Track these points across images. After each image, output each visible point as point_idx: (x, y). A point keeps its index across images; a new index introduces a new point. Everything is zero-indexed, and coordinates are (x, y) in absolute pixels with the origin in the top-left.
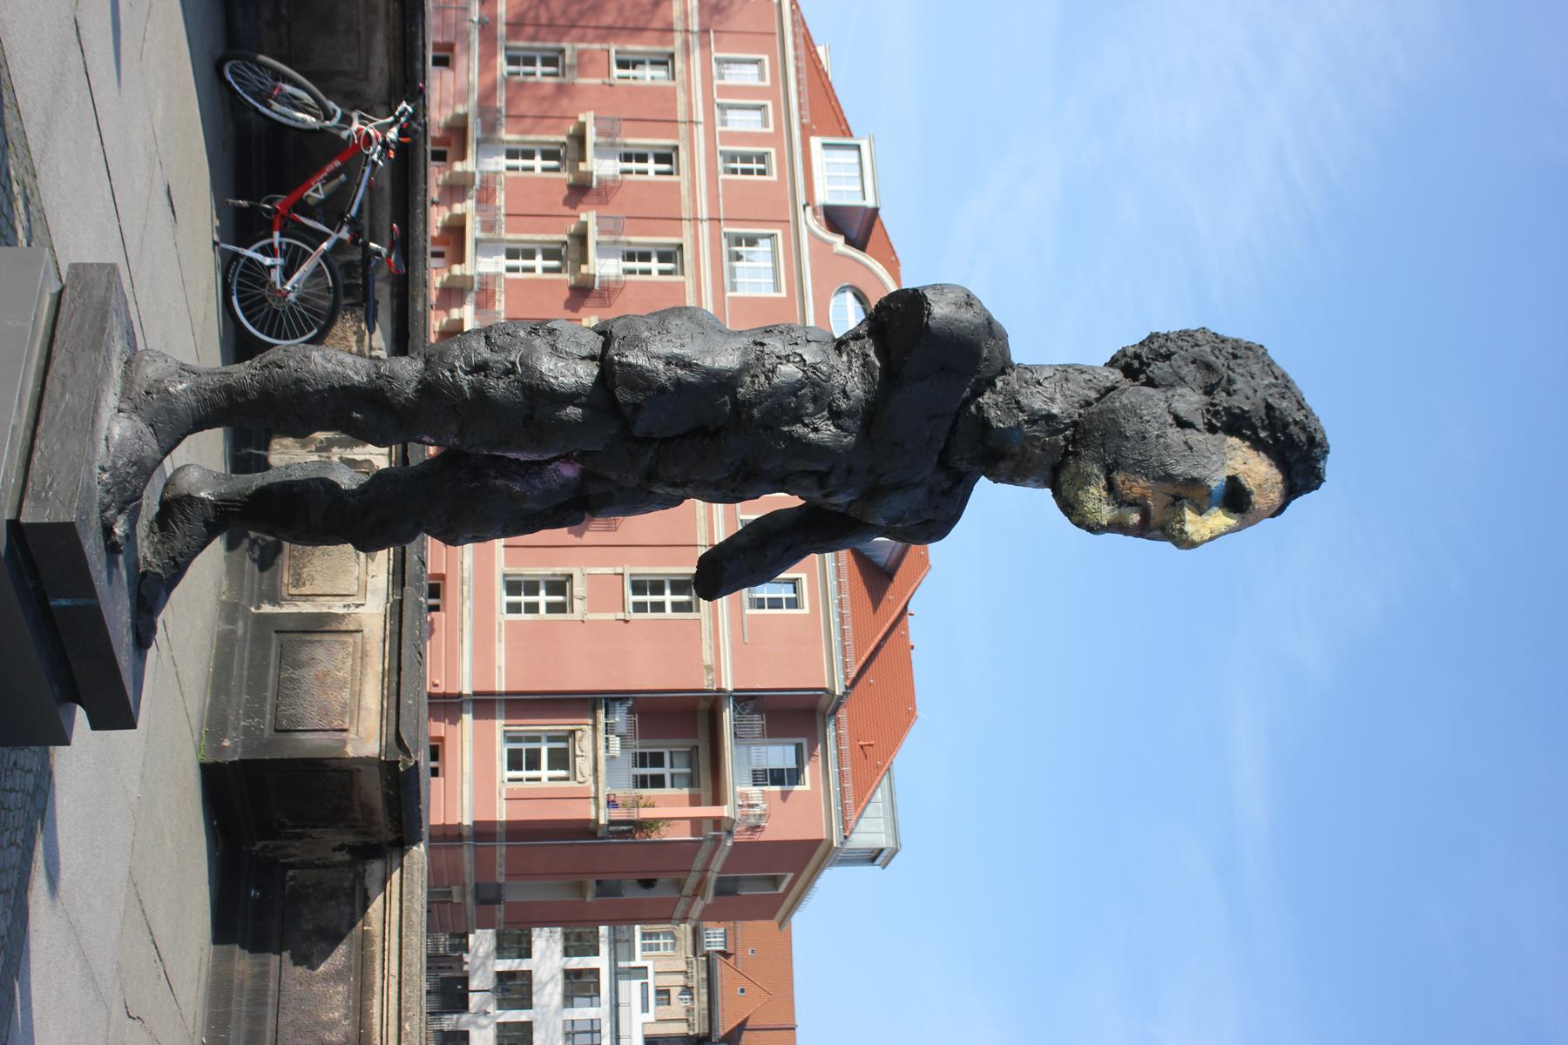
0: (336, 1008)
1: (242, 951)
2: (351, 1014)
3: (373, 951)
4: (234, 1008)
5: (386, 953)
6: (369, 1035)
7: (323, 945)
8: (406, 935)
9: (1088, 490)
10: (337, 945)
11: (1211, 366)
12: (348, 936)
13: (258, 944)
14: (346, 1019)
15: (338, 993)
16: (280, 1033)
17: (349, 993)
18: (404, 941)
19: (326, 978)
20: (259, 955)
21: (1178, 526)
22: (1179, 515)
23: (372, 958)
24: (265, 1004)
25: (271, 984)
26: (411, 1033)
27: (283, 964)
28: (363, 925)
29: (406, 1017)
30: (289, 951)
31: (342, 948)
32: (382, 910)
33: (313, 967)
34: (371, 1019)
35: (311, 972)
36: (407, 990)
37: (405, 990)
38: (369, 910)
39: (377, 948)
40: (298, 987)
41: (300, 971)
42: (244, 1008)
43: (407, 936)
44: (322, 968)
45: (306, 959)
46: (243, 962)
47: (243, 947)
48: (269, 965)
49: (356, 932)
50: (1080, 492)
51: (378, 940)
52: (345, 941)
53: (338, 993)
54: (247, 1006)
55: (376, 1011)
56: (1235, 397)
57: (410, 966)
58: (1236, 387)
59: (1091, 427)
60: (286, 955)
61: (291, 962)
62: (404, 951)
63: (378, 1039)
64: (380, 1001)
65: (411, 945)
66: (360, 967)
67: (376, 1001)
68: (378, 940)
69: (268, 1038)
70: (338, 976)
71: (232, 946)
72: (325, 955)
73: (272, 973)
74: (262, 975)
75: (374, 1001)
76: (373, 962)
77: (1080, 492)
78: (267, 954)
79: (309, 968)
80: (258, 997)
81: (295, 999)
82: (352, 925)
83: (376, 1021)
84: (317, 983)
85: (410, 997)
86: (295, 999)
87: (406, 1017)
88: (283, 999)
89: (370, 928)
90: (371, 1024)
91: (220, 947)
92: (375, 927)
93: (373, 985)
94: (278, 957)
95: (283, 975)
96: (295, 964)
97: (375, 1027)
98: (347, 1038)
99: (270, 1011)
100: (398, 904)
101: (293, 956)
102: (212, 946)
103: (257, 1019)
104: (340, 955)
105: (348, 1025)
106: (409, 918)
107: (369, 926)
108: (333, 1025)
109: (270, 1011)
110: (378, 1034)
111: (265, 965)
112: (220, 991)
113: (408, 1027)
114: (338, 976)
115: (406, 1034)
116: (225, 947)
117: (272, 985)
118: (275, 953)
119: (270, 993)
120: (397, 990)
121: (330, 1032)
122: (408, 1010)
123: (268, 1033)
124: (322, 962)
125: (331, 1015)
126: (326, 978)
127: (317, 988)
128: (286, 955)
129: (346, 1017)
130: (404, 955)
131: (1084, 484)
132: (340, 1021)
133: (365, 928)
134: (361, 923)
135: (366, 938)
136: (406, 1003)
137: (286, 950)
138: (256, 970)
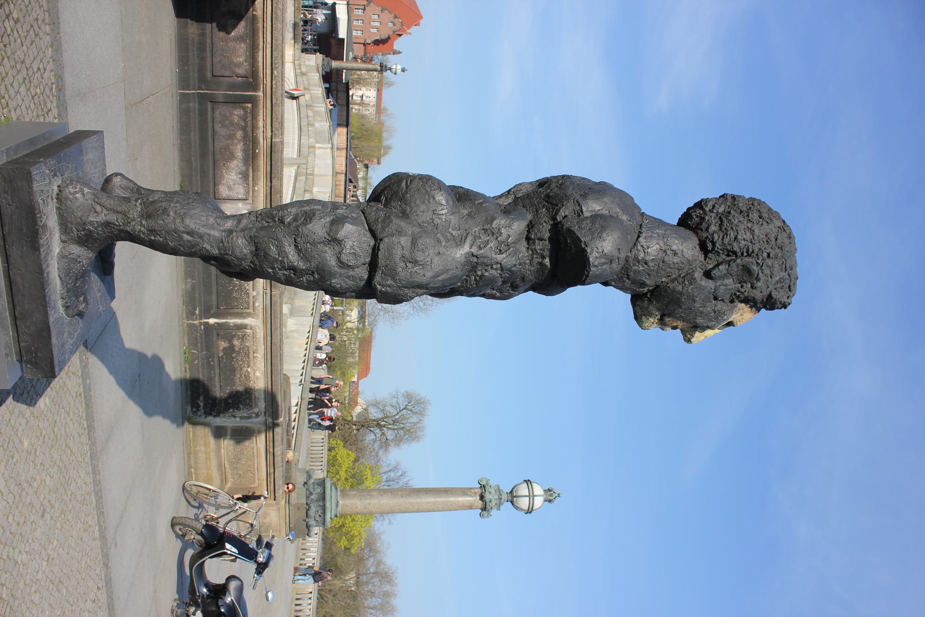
0: (241, 56)
1: (192, 22)
2: (248, 60)
3: (258, 26)
4: (190, 54)
5: (265, 29)
6: (257, 71)
7: (233, 20)
8: (275, 23)
9: (649, 319)
10: (240, 22)
11: (751, 272)
12: (246, 17)
13: (200, 18)
14: (246, 62)
15: (241, 48)
16: (214, 67)
17: (247, 48)
18: (274, 26)
19: (235, 39)
20: (200, 23)
21: (689, 336)
22: (692, 332)
23: (258, 30)
24: (205, 51)
25: (208, 40)
26: (277, 76)
27: (213, 30)
28: (253, 11)
29: (275, 68)
30: (216, 23)
31: (242, 24)
32: (262, 3)
33: (228, 33)
34: (258, 63)
35: (227, 35)
36: (276, 53)
37: (275, 54)
38: (256, 3)
39: (260, 25)
40: (221, 43)
41: (222, 34)
42: (196, 53)
43: (275, 23)
44: (233, 34)
45: (226, 28)
46: (193, 28)
47: (192, 19)
48: (206, 30)
49: (249, 14)
50: (644, 317)
51: (261, 20)
52: (244, 19)
53: (241, 48)
54: (197, 51)
55: (260, 59)
56: (754, 291)
57: (277, 40)
58: (759, 284)
59: (665, 295)
60: (214, 25)
61: (217, 29)
62: (274, 32)
63: (262, 74)
64: (262, 54)
65: (278, 28)
66: (252, 34)
67: (260, 54)
68: (261, 20)
69: (209, 69)
70: (241, 39)
71: (186, 20)
72: (234, 26)
73: (208, 33)
74: (203, 35)
75: (259, 54)
76: (258, 33)
77: (644, 317)
78: (205, 24)
79: (226, 33)
80: (202, 47)
81: (220, 49)
82: (247, 10)
83: (261, 64)
84: (231, 42)
85: (277, 57)
86: (220, 49)
87: (275, 68)
88: (215, 49)
89: (256, 13)
90: (258, 66)
91: (180, 19)
92: (259, 13)
93: (258, 45)
94: (210, 25)
95: (214, 35)
96: (219, 31)
97: (260, 67)
98: (247, 72)
99: (209, 54)
100: (270, 128)
101: (218, 26)
102: (176, 18)
103: (202, 59)
104: (241, 28)
105: (247, 65)
106: (276, 13)
107: (256, 12)
108: (239, 65)
109: (209, 54)
110: (262, 71)
111: (204, 29)
112: (183, 44)
113: (276, 73)
114: (241, 39)
115: (275, 76)
116: (183, 20)
117: (208, 40)
118: (208, 23)
119: (208, 45)
120: (270, 51)
121: (239, 68)
122: (276, 64)
123: (208, 66)
124: (233, 30)
125: (238, 59)
126: (235, 39)
127: (231, 44)
128: (214, 25)
129: (246, 61)
130: (273, 34)
131: (648, 315)
132: (243, 63)
133: (254, 13)
134: (251, 9)
135: (254, 18)
136: (275, 65)
137: (214, 22)
138: (200, 32)
